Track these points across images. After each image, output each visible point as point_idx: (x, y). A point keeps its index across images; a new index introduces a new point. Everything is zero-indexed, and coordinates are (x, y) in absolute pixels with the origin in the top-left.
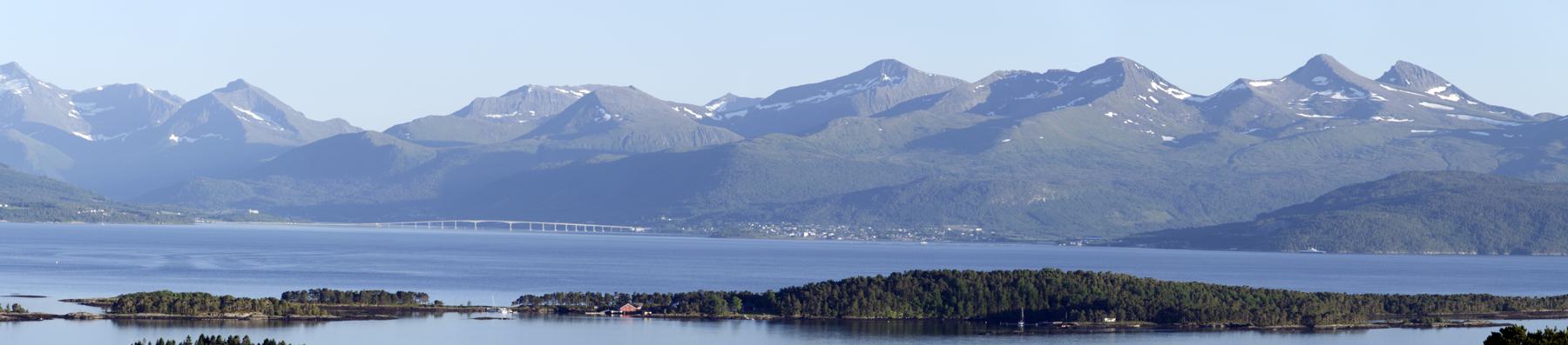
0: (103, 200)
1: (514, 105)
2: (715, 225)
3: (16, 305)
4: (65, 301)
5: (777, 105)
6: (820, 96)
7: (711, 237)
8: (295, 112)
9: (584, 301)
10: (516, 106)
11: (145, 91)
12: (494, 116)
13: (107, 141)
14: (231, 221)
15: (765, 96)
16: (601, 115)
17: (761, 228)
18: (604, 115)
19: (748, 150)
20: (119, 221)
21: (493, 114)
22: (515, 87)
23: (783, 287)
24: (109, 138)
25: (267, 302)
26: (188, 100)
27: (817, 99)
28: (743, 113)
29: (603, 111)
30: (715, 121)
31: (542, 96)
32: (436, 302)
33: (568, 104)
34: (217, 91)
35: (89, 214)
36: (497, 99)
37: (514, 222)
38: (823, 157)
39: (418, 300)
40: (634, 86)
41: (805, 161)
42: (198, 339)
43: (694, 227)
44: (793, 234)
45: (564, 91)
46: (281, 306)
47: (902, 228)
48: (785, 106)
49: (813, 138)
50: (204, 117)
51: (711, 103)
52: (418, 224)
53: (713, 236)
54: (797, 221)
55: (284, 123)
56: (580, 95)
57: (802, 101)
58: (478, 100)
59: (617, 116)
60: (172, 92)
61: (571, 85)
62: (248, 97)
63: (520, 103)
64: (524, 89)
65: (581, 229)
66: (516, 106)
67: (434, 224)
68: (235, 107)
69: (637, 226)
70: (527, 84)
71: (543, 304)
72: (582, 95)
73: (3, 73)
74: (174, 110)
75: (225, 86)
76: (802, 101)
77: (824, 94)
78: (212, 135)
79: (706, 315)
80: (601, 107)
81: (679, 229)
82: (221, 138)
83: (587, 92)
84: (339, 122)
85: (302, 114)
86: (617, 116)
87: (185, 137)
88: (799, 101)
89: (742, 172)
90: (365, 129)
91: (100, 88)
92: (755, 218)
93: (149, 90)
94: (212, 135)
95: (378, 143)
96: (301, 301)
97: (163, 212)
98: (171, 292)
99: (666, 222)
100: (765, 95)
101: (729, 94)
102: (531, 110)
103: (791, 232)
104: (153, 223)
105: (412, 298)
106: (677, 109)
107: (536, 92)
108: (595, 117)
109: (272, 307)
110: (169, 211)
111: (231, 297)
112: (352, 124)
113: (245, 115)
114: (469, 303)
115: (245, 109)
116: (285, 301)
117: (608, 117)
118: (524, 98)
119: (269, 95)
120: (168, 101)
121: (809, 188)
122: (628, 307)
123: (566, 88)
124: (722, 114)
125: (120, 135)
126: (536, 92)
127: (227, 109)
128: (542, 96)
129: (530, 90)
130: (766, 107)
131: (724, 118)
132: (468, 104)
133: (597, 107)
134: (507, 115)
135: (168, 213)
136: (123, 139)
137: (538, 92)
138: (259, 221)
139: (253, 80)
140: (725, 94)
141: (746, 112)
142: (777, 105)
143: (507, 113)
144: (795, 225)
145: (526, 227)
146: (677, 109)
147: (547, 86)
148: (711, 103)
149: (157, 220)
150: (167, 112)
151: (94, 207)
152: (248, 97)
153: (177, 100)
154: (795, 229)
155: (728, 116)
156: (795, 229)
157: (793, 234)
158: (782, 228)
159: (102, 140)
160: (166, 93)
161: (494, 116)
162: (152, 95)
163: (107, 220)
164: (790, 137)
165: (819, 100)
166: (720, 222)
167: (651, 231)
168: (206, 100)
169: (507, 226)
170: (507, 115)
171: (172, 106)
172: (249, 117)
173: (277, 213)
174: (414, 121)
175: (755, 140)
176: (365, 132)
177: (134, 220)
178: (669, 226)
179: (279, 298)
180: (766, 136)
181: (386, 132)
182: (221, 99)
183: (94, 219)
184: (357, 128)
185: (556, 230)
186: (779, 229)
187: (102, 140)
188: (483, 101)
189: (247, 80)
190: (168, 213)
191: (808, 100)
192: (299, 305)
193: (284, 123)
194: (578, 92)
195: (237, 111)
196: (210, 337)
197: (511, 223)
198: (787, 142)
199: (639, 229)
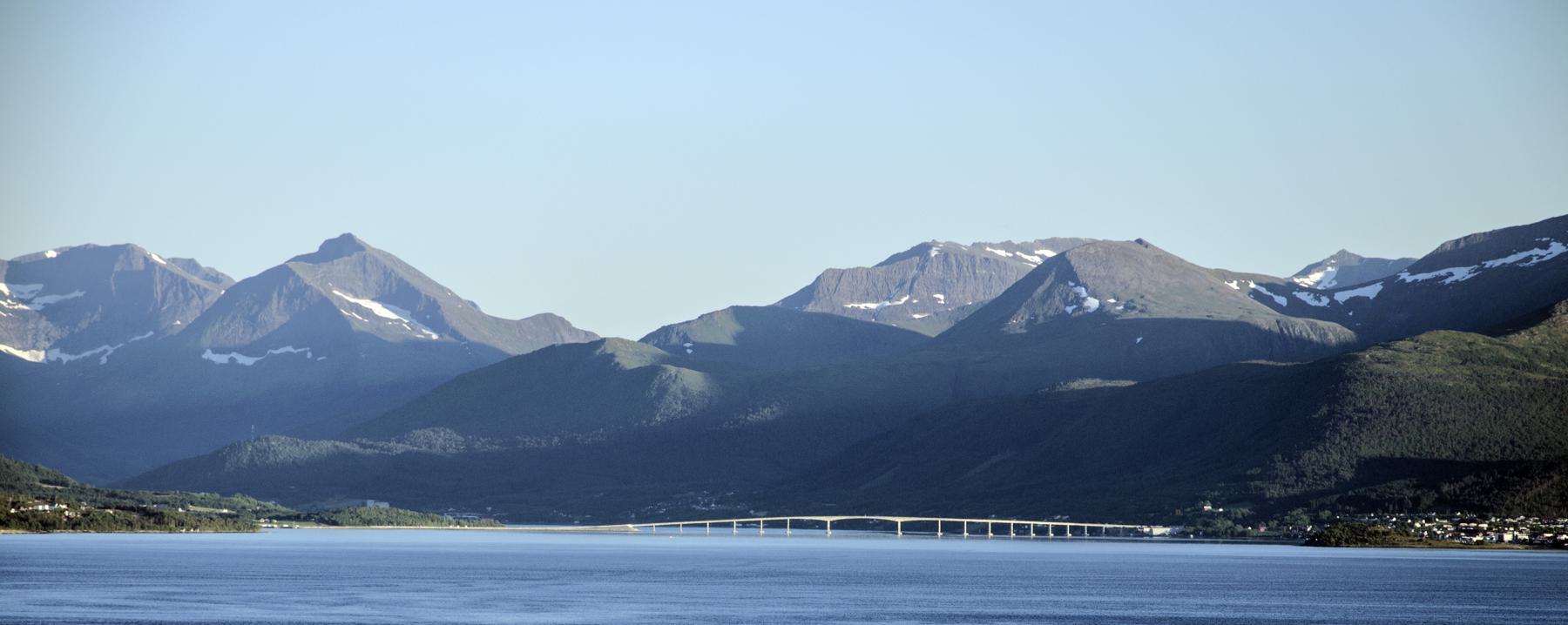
0: (67, 486)
1: (901, 285)
2: (1315, 521)
5: (1443, 272)
6: (1537, 251)
7: (1307, 544)
8: (459, 299)
10: (907, 285)
11: (147, 259)
12: (862, 306)
13: (69, 362)
14: (335, 523)
15: (1418, 254)
16: (1079, 301)
17: (1412, 526)
18: (1084, 299)
19: (1381, 366)
20: (100, 528)
21: (861, 301)
22: (904, 247)
24: (73, 358)
26: (238, 278)
27: (1529, 258)
28: (1371, 292)
29: (1083, 291)
30: (1316, 308)
31: (959, 266)
33: (1012, 280)
34: (297, 259)
35: (35, 513)
36: (868, 272)
37: (765, 519)
38: (1543, 377)
40: (1145, 238)
41: (1505, 385)
43: (1271, 523)
44: (1479, 538)
45: (1002, 253)
47: (45, 511)
48: (1461, 273)
49: (1521, 339)
50: (276, 315)
51: (1306, 272)
52: (712, 525)
54: (1488, 509)
55: (437, 323)
56: (1035, 260)
57: (1498, 262)
58: (830, 273)
59: (1112, 301)
60: (204, 263)
61: (1016, 241)
62: (365, 271)
63: (914, 280)
64: (922, 250)
65: (1041, 532)
66: (907, 285)
67: (744, 525)
68: (336, 292)
70: (929, 240)
72: (1039, 261)
73: (9, 280)
74: (210, 300)
75: (315, 249)
76: (1498, 262)
77: (1546, 246)
78: (290, 349)
80: (1078, 284)
81: (1240, 528)
82: (309, 355)
83: (1050, 254)
84: (549, 321)
85: (474, 305)
86: (1112, 301)
87: (234, 355)
88: (1489, 264)
89: (1371, 411)
90: (602, 335)
91: (51, 254)
92: (1400, 506)
93: (155, 258)
94: (290, 349)
95: (629, 362)
97: (191, 508)
99: (1211, 515)
100: (1419, 252)
101: (1343, 253)
102: (939, 292)
103: (1475, 532)
104: (171, 531)
106: (1234, 285)
107: (946, 256)
108: (1067, 304)
110: (202, 505)
112: (575, 324)
113: (358, 309)
115: (356, 296)
117: (1093, 303)
118: (922, 268)
119: (408, 268)
120: (196, 279)
121: (1512, 442)
123: (1007, 246)
124: (1329, 293)
125: (98, 351)
126: (946, 256)
127: (320, 294)
128: (959, 266)
129: (934, 253)
130: (1421, 277)
131: (1333, 302)
132: (809, 282)
133: (1071, 284)
134: (888, 303)
135: (199, 509)
136: (104, 360)
137: (950, 254)
138: (391, 523)
139: (374, 237)
140: (1334, 252)
141: (1378, 287)
142: (1443, 272)
143: (889, 299)
144: (1484, 518)
145: (930, 528)
146: (1234, 285)
147: (969, 244)
148: (1306, 272)
149: (181, 524)
150: (196, 302)
151: (44, 499)
152: (365, 271)
153: (215, 278)
154: (1485, 526)
155: (1341, 297)
156: (1485, 526)
157: (1479, 538)
158: (1456, 525)
159: (59, 360)
160: (191, 265)
161: (862, 306)
162: (163, 269)
163: (73, 525)
164: (1471, 337)
165: (1535, 260)
166: (1326, 514)
167: (1185, 534)
168: (278, 276)
169: (892, 527)
170: (888, 303)
171: (206, 290)
172: (368, 313)
173: (872, 520)
174: (701, 317)
175: (1400, 344)
176: (603, 341)
177: (130, 525)
178: (1221, 524)
180: (1423, 337)
181: (645, 340)
182: (305, 274)
183: (46, 525)
184: (587, 334)
185: (991, 534)
186: (1451, 528)
187: (59, 360)
188: (838, 275)
189: (361, 236)
190: (199, 509)
191: (1511, 259)
193: (437, 323)
194: (1034, 255)
195: (339, 298)
198: (1467, 348)
199: (1158, 530)
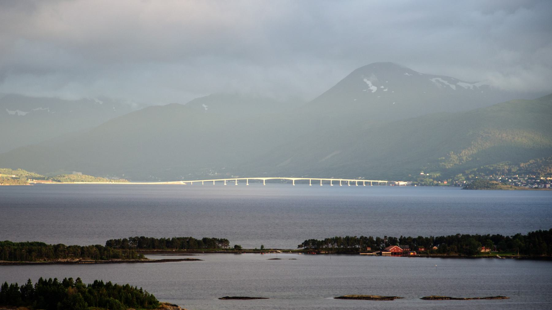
3: (71, 278)
4: (296, 259)
9: (359, 244)
23: (215, 237)
25: (94, 249)
32: (236, 246)
39: (220, 245)
42: (37, 281)
46: (106, 252)
53: (466, 187)
69: (400, 180)
71: (324, 247)
79: (327, 252)
82: (49, 111)
96: (122, 247)
98: (11, 242)
99: (424, 177)
105: (215, 243)
109: (98, 252)
111: (63, 245)
114: (262, 247)
116: (109, 248)
122: (393, 248)
179: (104, 245)
192: (120, 251)
196: (48, 280)
197: (294, 179)
199: (401, 183)
